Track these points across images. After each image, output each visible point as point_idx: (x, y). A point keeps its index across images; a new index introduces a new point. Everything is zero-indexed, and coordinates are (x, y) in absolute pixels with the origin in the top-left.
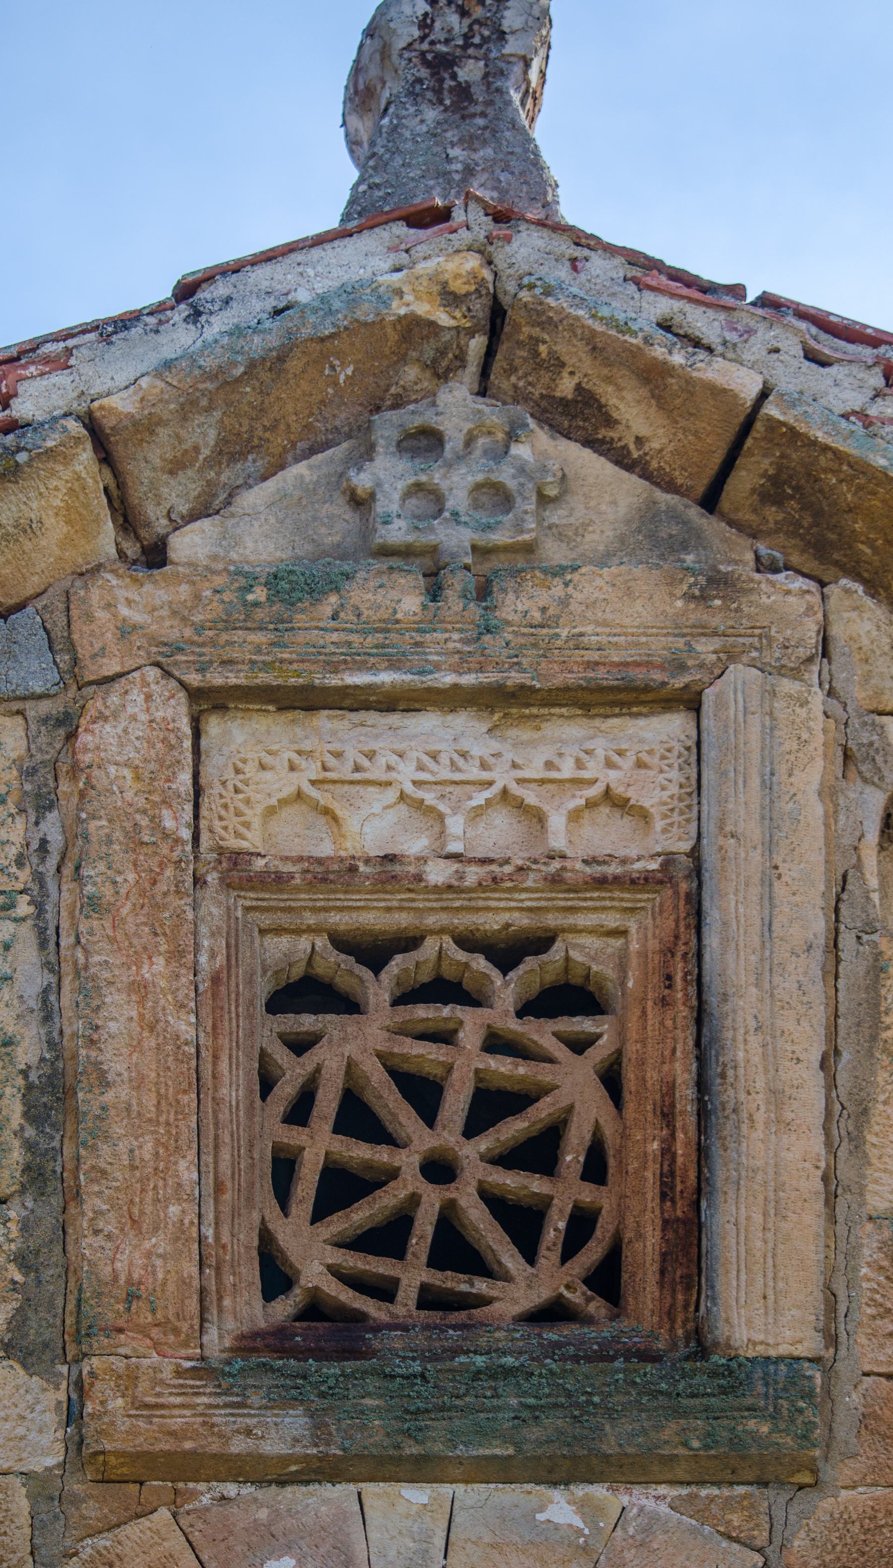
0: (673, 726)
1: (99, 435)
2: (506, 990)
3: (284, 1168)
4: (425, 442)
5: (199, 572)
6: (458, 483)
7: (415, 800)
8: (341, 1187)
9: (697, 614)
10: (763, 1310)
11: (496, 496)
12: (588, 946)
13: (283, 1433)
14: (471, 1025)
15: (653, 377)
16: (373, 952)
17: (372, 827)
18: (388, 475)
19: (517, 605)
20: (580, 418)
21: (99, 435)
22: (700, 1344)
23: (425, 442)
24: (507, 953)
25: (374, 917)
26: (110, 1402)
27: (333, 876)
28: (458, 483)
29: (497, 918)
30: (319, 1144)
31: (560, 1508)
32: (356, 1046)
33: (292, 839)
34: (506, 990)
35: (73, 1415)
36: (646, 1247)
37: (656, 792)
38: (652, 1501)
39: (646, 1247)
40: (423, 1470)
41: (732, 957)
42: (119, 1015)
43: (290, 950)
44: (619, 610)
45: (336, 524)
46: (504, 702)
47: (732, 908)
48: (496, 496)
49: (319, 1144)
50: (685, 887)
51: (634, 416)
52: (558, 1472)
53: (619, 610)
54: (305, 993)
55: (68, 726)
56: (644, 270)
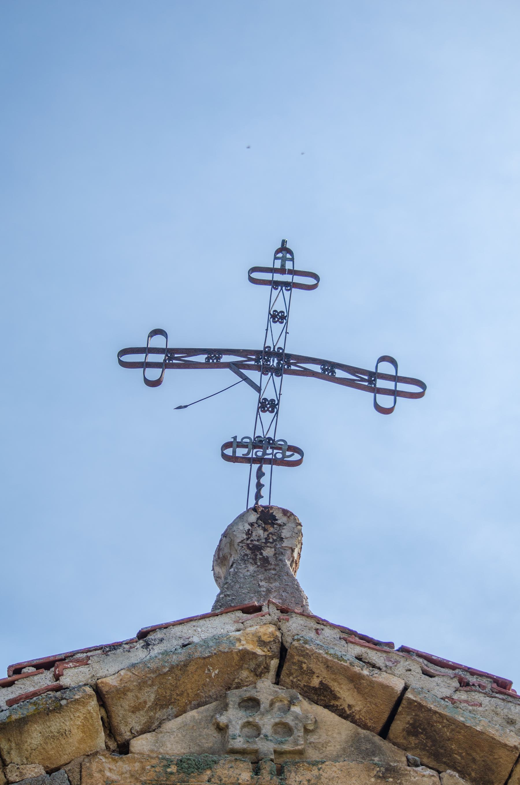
5: (144, 757)
6: (267, 723)
11: (285, 729)
15: (355, 680)
18: (234, 717)
20: (323, 696)
23: (252, 704)
28: (267, 723)
45: (210, 738)
48: (285, 729)
51: (347, 696)
56: (348, 635)
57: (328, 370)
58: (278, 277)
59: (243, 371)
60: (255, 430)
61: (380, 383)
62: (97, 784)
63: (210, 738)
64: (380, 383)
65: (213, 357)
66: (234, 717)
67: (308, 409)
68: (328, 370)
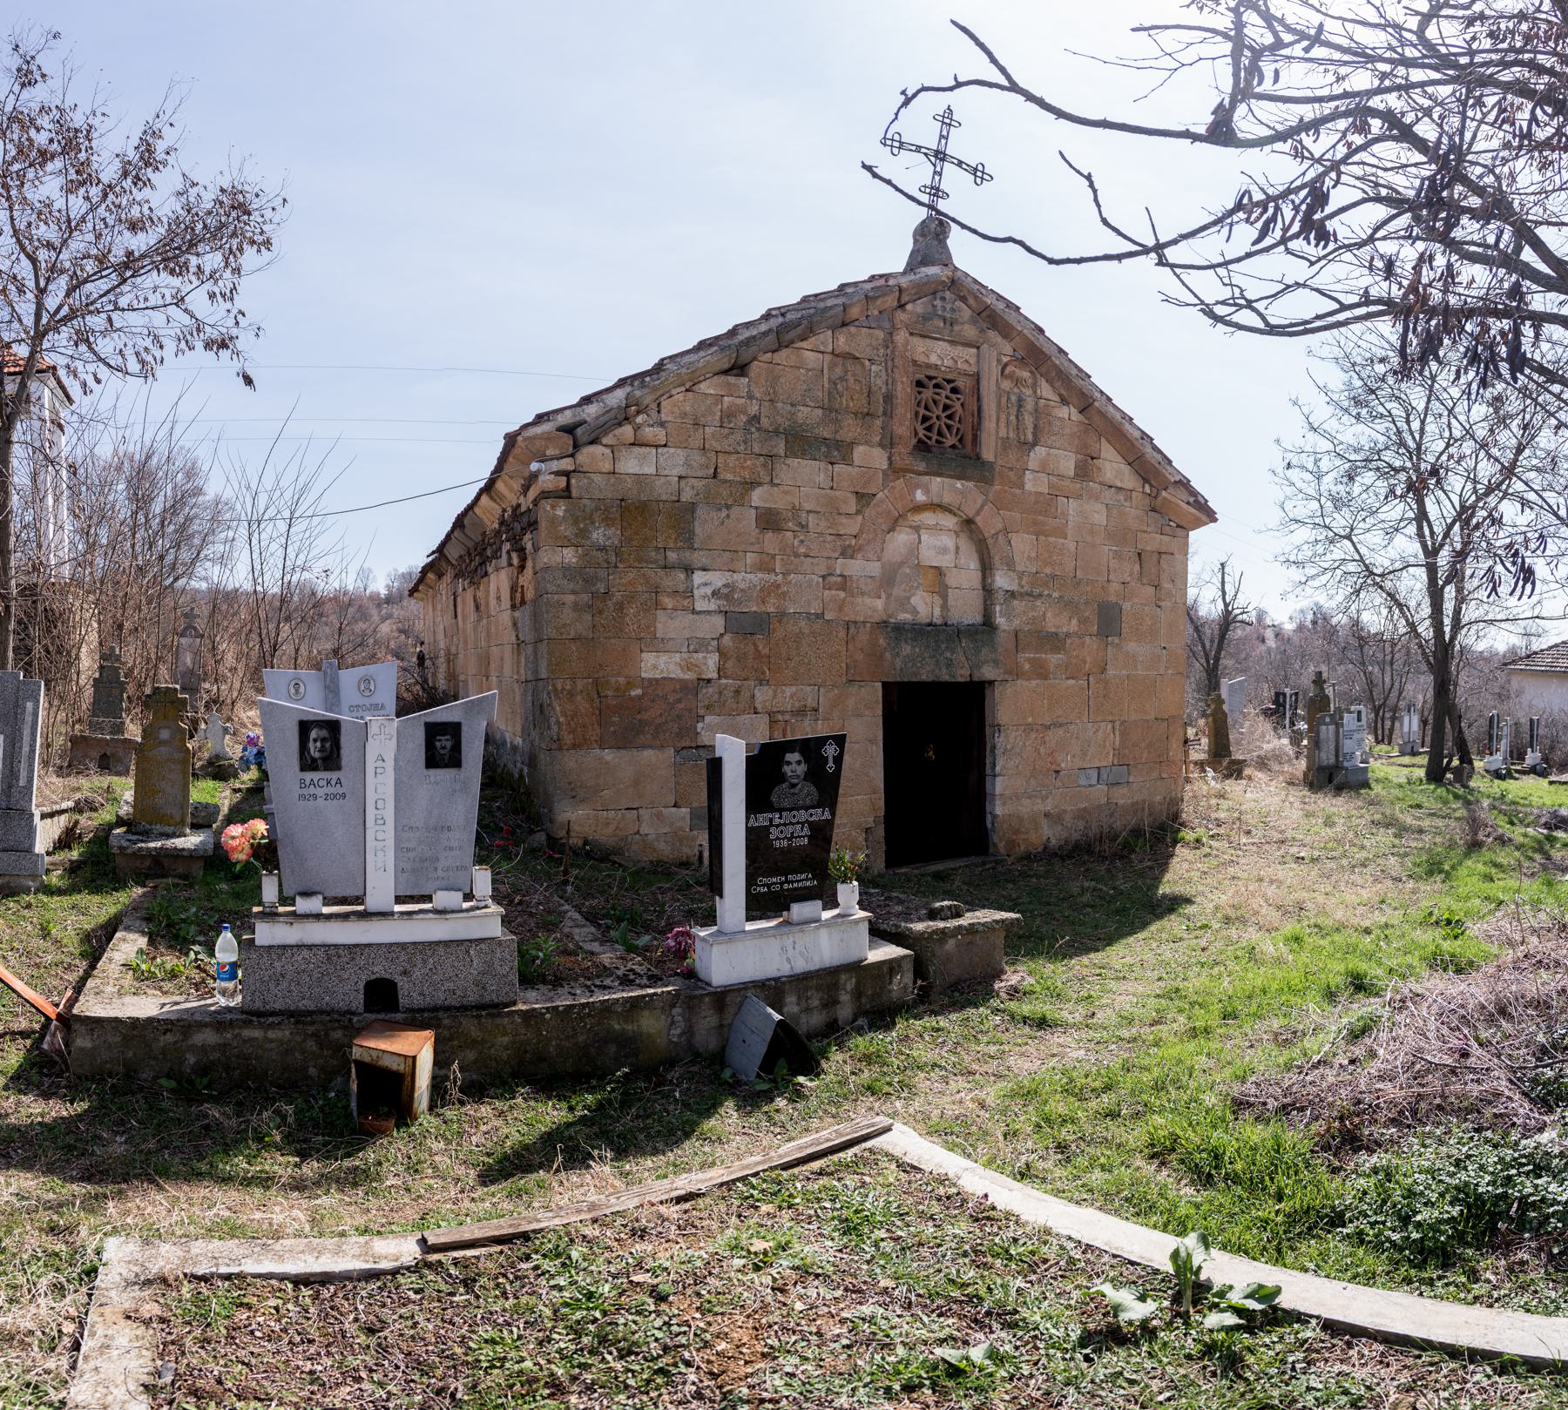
0: (974, 351)
1: (900, 290)
2: (948, 387)
3: (917, 413)
4: (943, 299)
5: (912, 313)
6: (948, 307)
7: (939, 354)
8: (925, 419)
9: (1397, 841)
10: (988, 454)
11: (953, 310)
12: (960, 383)
13: (922, 466)
14: (944, 393)
15: (976, 298)
16: (930, 378)
17: (934, 359)
18: (938, 303)
19: (956, 328)
20: (963, 299)
21: (900, 290)
22: (978, 458)
23: (943, 299)
24: (949, 381)
25: (932, 373)
26: (896, 458)
27: (928, 366)
28: (948, 307)
29: (949, 377)
30: (922, 411)
31: (959, 485)
32: (928, 394)
33: (921, 359)
34: (948, 387)
35: (889, 459)
36: (969, 438)
37: (973, 361)
38: (971, 484)
39: (969, 438)
40: (940, 475)
41: (984, 392)
42: (899, 388)
43: (921, 376)
44: (970, 332)
45: (930, 309)
46: (952, 343)
47: (984, 383)
48: (953, 310)
49: (922, 411)
50: (977, 378)
51: (971, 301)
52: (959, 478)
53: (970, 332)
54: (919, 384)
55: (891, 334)
56: (975, 281)
57: (960, 164)
58: (1341, 317)
59: (1447, 637)
60: (975, 232)
61: (979, 174)
62: (1378, 1402)
63: (930, 309)
64: (979, 174)
65: (918, 149)
66: (938, 303)
67: (953, 178)
68: (960, 164)
